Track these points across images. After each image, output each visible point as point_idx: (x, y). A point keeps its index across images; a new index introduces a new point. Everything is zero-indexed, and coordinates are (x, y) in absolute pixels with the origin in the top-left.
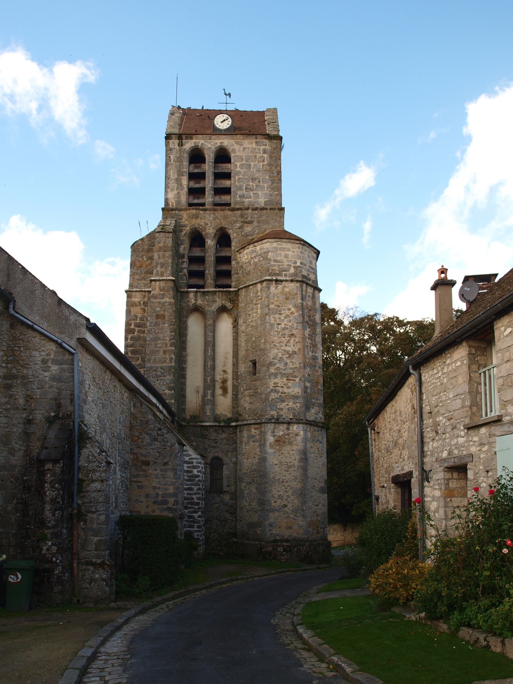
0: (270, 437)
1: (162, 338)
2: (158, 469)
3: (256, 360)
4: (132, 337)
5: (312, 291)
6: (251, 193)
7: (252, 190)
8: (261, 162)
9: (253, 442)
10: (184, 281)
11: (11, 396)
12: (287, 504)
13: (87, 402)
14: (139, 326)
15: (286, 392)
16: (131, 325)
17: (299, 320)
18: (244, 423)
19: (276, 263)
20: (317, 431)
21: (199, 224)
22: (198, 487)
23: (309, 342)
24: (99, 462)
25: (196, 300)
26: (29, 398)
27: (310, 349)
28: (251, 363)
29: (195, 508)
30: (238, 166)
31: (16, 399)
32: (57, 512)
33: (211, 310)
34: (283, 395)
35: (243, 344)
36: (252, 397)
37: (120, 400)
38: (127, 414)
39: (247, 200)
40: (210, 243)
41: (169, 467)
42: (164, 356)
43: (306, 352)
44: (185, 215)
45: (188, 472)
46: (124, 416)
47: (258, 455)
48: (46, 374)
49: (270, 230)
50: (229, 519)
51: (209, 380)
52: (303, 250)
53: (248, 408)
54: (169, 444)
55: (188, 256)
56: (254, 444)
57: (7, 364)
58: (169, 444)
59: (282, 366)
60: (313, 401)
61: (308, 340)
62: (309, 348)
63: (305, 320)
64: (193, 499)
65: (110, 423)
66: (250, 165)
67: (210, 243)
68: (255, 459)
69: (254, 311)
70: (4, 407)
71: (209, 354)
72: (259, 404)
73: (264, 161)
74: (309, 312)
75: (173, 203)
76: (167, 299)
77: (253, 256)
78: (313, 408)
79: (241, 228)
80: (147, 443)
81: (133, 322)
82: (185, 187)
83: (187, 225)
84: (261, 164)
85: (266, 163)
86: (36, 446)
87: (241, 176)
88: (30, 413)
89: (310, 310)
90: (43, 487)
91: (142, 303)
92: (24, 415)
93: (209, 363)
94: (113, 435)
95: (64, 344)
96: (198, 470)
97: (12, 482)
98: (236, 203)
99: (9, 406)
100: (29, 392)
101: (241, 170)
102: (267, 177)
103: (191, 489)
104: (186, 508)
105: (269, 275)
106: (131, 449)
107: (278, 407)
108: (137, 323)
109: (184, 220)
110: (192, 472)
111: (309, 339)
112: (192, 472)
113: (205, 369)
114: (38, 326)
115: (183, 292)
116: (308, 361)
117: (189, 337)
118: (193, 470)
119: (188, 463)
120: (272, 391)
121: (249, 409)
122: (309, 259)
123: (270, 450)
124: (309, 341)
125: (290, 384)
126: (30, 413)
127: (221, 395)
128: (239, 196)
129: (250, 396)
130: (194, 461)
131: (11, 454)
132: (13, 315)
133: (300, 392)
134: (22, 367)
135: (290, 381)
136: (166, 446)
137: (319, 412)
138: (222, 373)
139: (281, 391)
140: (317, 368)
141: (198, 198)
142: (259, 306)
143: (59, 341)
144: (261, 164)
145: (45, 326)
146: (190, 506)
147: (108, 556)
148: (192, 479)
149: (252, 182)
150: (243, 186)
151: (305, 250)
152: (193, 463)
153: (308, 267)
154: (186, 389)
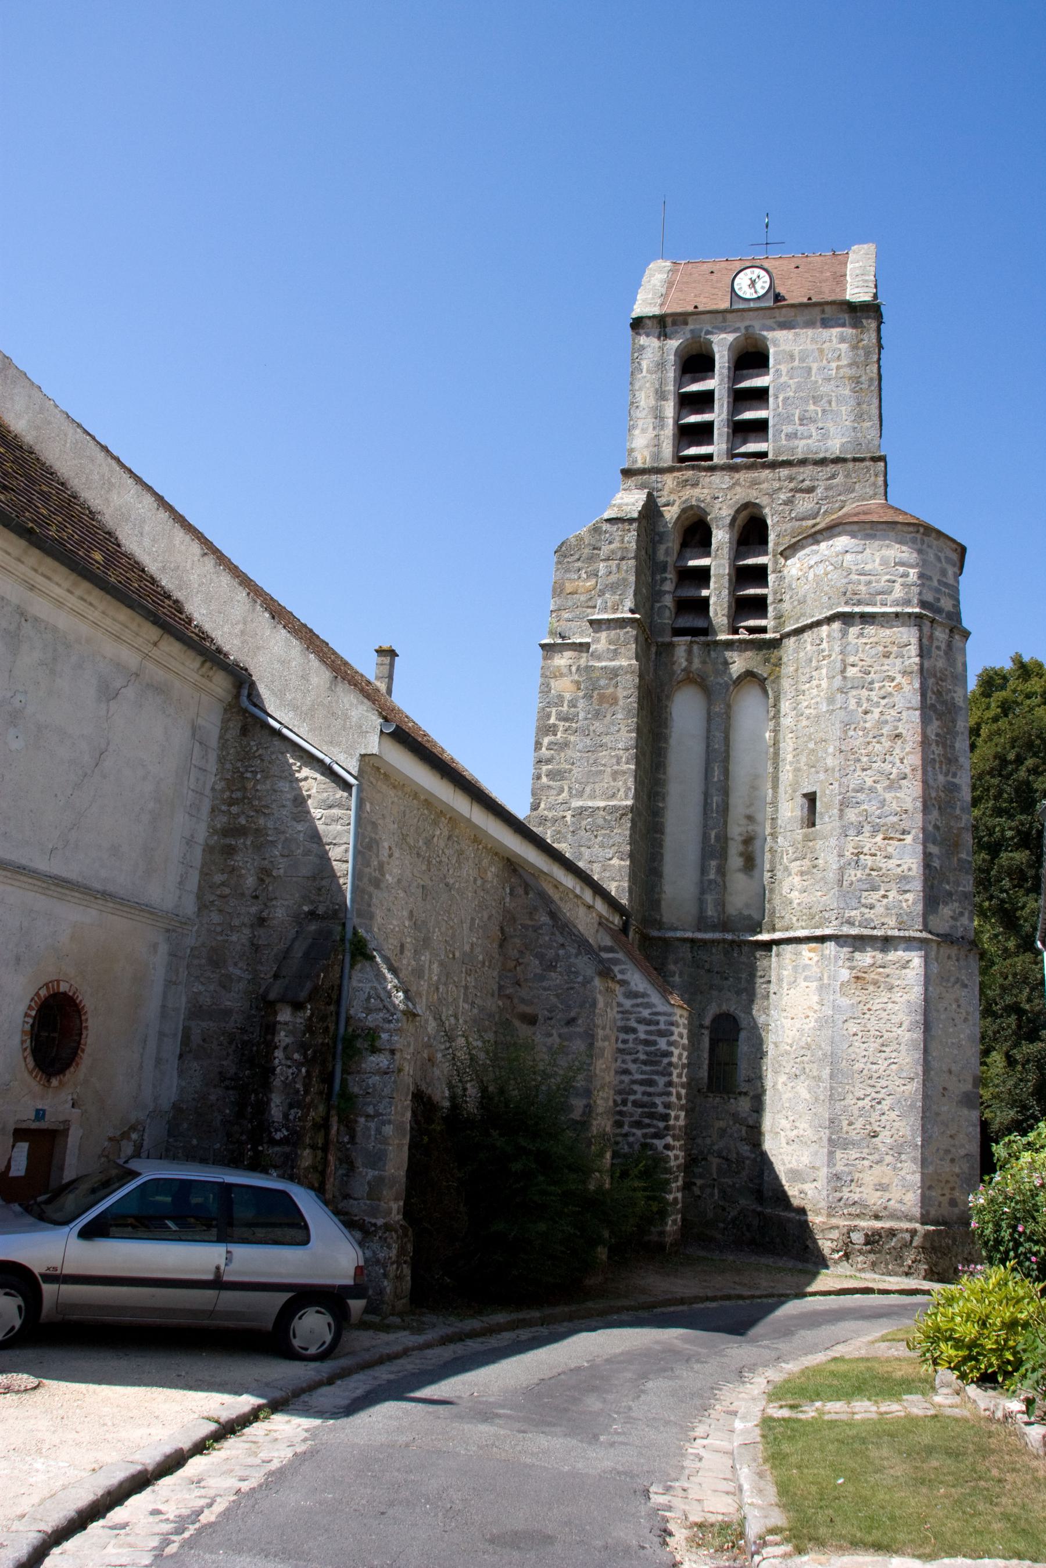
0: (843, 970)
1: (609, 745)
2: (554, 1032)
3: (815, 793)
4: (551, 743)
5: (946, 637)
6: (812, 428)
7: (812, 420)
8: (834, 361)
9: (805, 980)
10: (667, 618)
11: (233, 870)
12: (878, 1129)
13: (383, 885)
14: (566, 719)
15: (881, 865)
16: (549, 716)
17: (914, 701)
18: (777, 935)
19: (862, 578)
20: (954, 958)
21: (698, 500)
22: (666, 1079)
23: (937, 752)
24: (388, 1011)
25: (690, 661)
26: (264, 874)
27: (941, 768)
28: (805, 800)
29: (658, 1127)
30: (784, 373)
31: (240, 876)
32: (292, 1111)
33: (722, 681)
34: (874, 873)
35: (789, 757)
36: (805, 878)
37: (475, 880)
38: (494, 912)
39: (803, 442)
40: (721, 537)
41: (578, 1029)
42: (612, 784)
43: (930, 773)
44: (669, 481)
45: (647, 1043)
46: (486, 915)
47: (815, 1011)
48: (300, 828)
49: (854, 505)
50: (748, 1158)
51: (713, 836)
52: (925, 547)
53: (798, 901)
54: (580, 979)
55: (675, 567)
56: (806, 984)
57: (230, 805)
58: (580, 979)
59: (871, 807)
60: (947, 887)
61: (934, 747)
62: (937, 766)
63: (929, 702)
64: (654, 1105)
65: (443, 929)
66: (810, 368)
67: (721, 537)
68: (808, 1020)
69: (814, 683)
70: (218, 892)
71: (716, 779)
72: (820, 893)
73: (839, 358)
74: (937, 683)
76: (624, 663)
77: (812, 562)
78: (946, 904)
79: (789, 502)
80: (535, 975)
81: (554, 710)
82: (670, 422)
84: (834, 365)
85: (844, 362)
86: (267, 970)
87: (791, 394)
88: (265, 905)
89: (942, 680)
90: (269, 1056)
91: (574, 669)
92: (253, 910)
93: (715, 799)
94: (451, 956)
95: (336, 767)
96: (668, 1041)
97: (221, 1044)
98: (778, 453)
99: (227, 891)
100: (266, 862)
101: (791, 381)
102: (847, 392)
103: (650, 1083)
104: (638, 1124)
105: (846, 603)
106: (501, 988)
107: (863, 901)
108: (561, 711)
109: (665, 493)
110: (655, 1043)
111: (938, 745)
112: (655, 1043)
113: (705, 813)
114: (291, 730)
115: (663, 644)
116: (933, 795)
117: (673, 741)
118: (658, 1039)
119: (649, 1023)
120: (850, 864)
121: (799, 904)
122: (939, 565)
123: (842, 999)
124: (939, 750)
125: (890, 849)
126: (265, 905)
127: (740, 870)
128: (787, 435)
129: (802, 873)
130: (662, 1019)
131: (224, 987)
132: (245, 711)
133: (914, 867)
134: (257, 811)
135: (891, 842)
136: (575, 983)
137: (961, 914)
138: (744, 821)
139: (870, 863)
140: (958, 812)
141: (699, 444)
142: (824, 671)
143: (328, 761)
144: (834, 365)
145: (301, 731)
146: (647, 1121)
147: (398, 1213)
148: (654, 1059)
149: (814, 403)
150: (793, 415)
151: (929, 546)
152: (657, 1023)
153: (935, 583)
154: (662, 855)
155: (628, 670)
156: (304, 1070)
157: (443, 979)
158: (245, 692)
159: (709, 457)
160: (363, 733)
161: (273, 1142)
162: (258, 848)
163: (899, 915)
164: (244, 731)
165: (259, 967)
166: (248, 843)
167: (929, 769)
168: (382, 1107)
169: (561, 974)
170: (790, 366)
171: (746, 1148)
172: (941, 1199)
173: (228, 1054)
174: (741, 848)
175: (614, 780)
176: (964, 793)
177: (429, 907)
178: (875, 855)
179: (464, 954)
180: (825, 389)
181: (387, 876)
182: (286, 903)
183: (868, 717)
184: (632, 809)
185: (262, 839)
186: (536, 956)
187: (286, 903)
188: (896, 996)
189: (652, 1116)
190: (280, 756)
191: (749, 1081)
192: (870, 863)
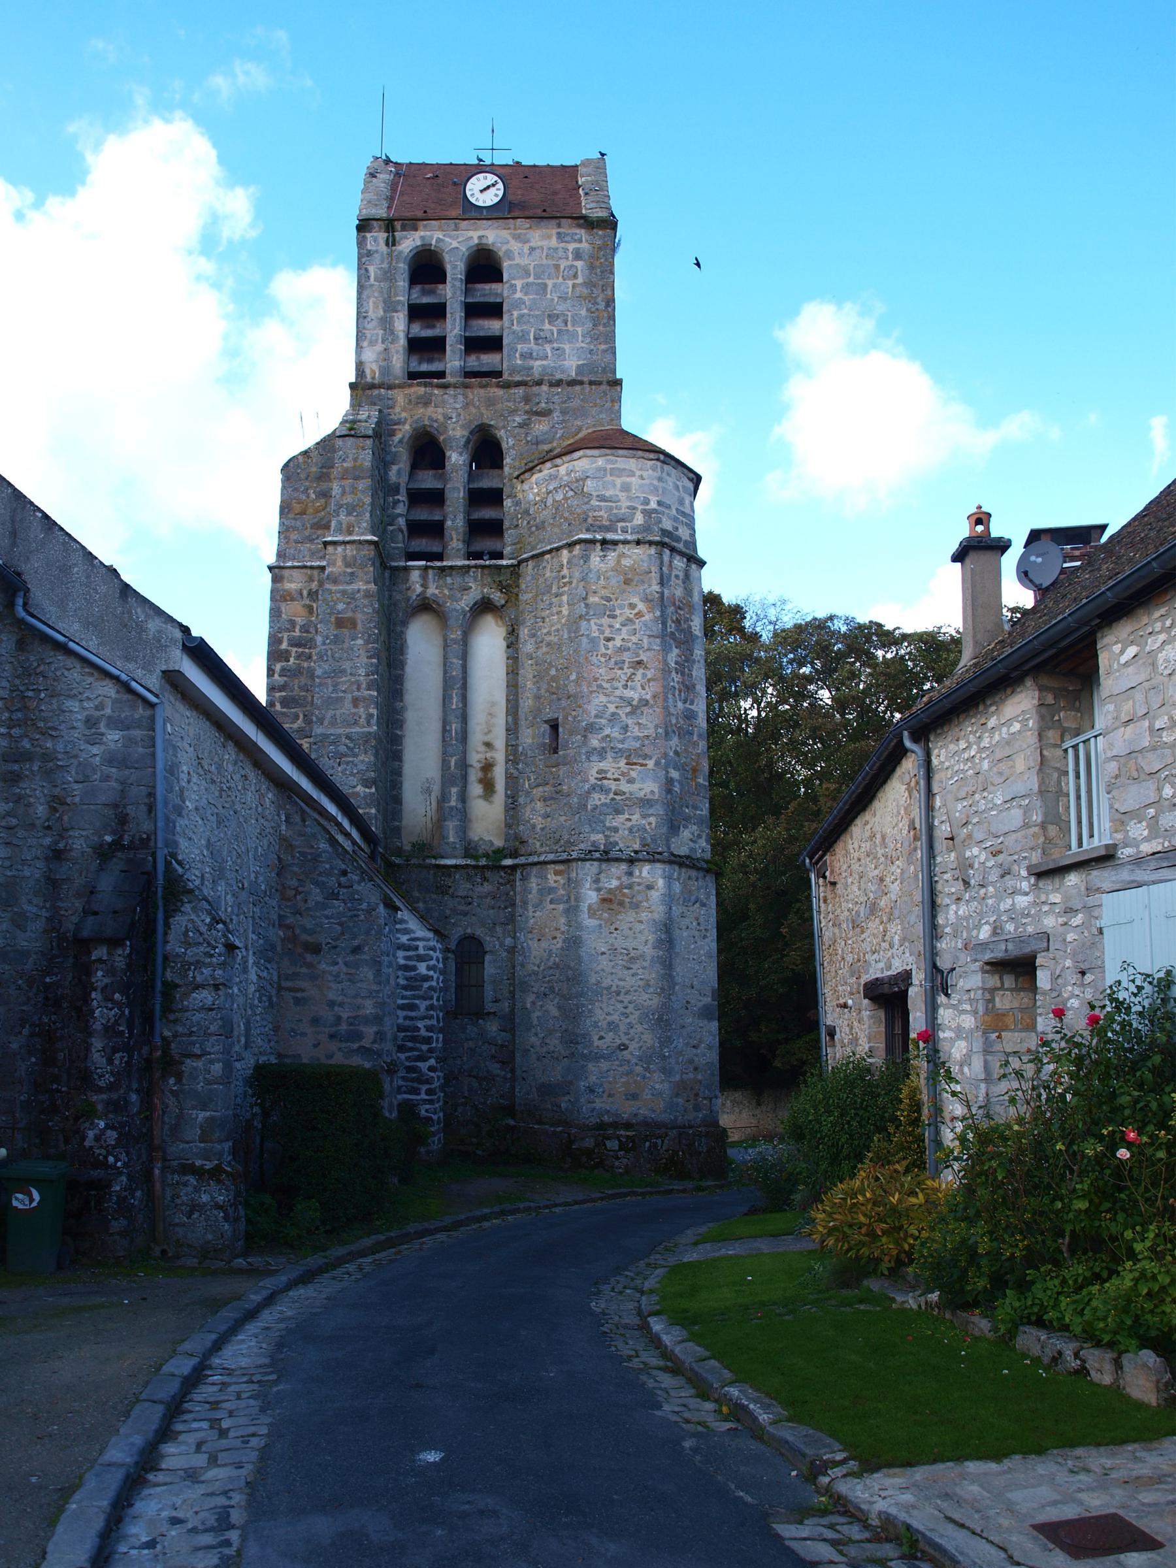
1: (349, 671)
2: (340, 960)
4: (283, 669)
9: (551, 902)
11: (19, 799)
12: (627, 1042)
13: (184, 812)
16: (280, 641)
19: (602, 504)
22: (428, 1003)
25: (425, 586)
26: (57, 803)
29: (421, 1050)
30: (518, 288)
31: (29, 805)
35: (529, 684)
36: (548, 803)
39: (538, 363)
40: (456, 458)
41: (365, 957)
45: (406, 968)
46: (265, 842)
47: (563, 933)
48: (95, 750)
51: (453, 764)
52: (664, 474)
54: (364, 906)
56: (553, 906)
57: (10, 728)
58: (364, 906)
59: (616, 733)
61: (674, 674)
66: (546, 285)
67: (456, 458)
69: (555, 610)
73: (575, 276)
75: (373, 371)
76: (360, 585)
77: (551, 488)
78: (685, 827)
81: (286, 635)
83: (406, 419)
84: (570, 283)
85: (580, 280)
87: (526, 311)
89: (680, 608)
91: (305, 593)
92: (47, 841)
93: (454, 727)
95: (134, 684)
99: (14, 821)
100: (58, 789)
103: (413, 1007)
105: (588, 530)
107: (608, 824)
109: (397, 409)
110: (414, 968)
112: (414, 968)
115: (397, 568)
116: (674, 721)
117: (409, 669)
118: (418, 964)
121: (542, 829)
122: (677, 493)
125: (633, 774)
126: (60, 835)
127: (480, 797)
128: (521, 355)
130: (421, 944)
131: (19, 927)
133: (656, 790)
137: (699, 836)
138: (482, 748)
139: (613, 788)
140: (695, 738)
142: (565, 598)
143: (124, 677)
144: (570, 283)
145: (93, 644)
146: (410, 1044)
149: (550, 323)
150: (528, 334)
151: (669, 475)
152: (417, 948)
153: (674, 512)
155: (368, 594)
156: (127, 1012)
157: (236, 911)
158: (20, 601)
159: (441, 375)
160: (163, 648)
161: (100, 1090)
162: (48, 774)
163: (642, 839)
164: (21, 645)
165: (60, 904)
166: (36, 768)
167: (670, 696)
168: (210, 1044)
169: (344, 901)
170: (526, 281)
171: (497, 1066)
172: (687, 1105)
173: (29, 999)
174: (480, 775)
175: (355, 706)
176: (700, 720)
177: (222, 835)
178: (618, 780)
179: (251, 883)
180: (560, 308)
181: (187, 803)
182: (84, 833)
183: (610, 644)
184: (376, 736)
185: (51, 764)
186: (317, 884)
187: (84, 833)
188: (644, 916)
189: (414, 1039)
190: (66, 673)
191: (496, 1002)
192: (613, 788)
